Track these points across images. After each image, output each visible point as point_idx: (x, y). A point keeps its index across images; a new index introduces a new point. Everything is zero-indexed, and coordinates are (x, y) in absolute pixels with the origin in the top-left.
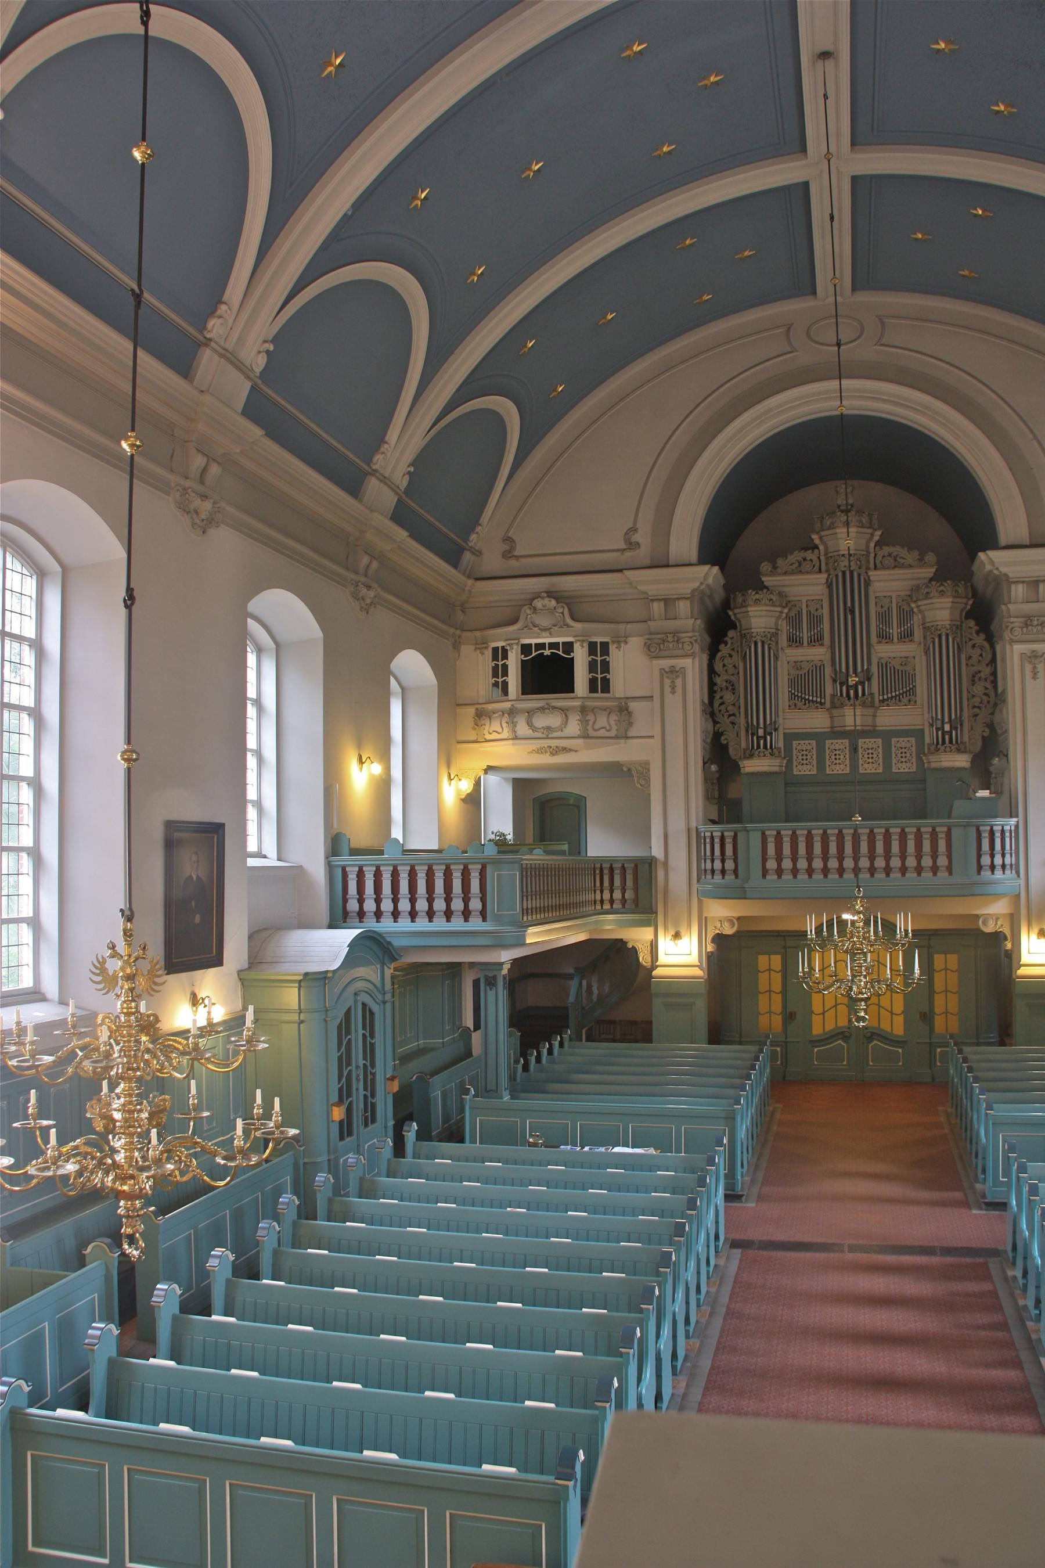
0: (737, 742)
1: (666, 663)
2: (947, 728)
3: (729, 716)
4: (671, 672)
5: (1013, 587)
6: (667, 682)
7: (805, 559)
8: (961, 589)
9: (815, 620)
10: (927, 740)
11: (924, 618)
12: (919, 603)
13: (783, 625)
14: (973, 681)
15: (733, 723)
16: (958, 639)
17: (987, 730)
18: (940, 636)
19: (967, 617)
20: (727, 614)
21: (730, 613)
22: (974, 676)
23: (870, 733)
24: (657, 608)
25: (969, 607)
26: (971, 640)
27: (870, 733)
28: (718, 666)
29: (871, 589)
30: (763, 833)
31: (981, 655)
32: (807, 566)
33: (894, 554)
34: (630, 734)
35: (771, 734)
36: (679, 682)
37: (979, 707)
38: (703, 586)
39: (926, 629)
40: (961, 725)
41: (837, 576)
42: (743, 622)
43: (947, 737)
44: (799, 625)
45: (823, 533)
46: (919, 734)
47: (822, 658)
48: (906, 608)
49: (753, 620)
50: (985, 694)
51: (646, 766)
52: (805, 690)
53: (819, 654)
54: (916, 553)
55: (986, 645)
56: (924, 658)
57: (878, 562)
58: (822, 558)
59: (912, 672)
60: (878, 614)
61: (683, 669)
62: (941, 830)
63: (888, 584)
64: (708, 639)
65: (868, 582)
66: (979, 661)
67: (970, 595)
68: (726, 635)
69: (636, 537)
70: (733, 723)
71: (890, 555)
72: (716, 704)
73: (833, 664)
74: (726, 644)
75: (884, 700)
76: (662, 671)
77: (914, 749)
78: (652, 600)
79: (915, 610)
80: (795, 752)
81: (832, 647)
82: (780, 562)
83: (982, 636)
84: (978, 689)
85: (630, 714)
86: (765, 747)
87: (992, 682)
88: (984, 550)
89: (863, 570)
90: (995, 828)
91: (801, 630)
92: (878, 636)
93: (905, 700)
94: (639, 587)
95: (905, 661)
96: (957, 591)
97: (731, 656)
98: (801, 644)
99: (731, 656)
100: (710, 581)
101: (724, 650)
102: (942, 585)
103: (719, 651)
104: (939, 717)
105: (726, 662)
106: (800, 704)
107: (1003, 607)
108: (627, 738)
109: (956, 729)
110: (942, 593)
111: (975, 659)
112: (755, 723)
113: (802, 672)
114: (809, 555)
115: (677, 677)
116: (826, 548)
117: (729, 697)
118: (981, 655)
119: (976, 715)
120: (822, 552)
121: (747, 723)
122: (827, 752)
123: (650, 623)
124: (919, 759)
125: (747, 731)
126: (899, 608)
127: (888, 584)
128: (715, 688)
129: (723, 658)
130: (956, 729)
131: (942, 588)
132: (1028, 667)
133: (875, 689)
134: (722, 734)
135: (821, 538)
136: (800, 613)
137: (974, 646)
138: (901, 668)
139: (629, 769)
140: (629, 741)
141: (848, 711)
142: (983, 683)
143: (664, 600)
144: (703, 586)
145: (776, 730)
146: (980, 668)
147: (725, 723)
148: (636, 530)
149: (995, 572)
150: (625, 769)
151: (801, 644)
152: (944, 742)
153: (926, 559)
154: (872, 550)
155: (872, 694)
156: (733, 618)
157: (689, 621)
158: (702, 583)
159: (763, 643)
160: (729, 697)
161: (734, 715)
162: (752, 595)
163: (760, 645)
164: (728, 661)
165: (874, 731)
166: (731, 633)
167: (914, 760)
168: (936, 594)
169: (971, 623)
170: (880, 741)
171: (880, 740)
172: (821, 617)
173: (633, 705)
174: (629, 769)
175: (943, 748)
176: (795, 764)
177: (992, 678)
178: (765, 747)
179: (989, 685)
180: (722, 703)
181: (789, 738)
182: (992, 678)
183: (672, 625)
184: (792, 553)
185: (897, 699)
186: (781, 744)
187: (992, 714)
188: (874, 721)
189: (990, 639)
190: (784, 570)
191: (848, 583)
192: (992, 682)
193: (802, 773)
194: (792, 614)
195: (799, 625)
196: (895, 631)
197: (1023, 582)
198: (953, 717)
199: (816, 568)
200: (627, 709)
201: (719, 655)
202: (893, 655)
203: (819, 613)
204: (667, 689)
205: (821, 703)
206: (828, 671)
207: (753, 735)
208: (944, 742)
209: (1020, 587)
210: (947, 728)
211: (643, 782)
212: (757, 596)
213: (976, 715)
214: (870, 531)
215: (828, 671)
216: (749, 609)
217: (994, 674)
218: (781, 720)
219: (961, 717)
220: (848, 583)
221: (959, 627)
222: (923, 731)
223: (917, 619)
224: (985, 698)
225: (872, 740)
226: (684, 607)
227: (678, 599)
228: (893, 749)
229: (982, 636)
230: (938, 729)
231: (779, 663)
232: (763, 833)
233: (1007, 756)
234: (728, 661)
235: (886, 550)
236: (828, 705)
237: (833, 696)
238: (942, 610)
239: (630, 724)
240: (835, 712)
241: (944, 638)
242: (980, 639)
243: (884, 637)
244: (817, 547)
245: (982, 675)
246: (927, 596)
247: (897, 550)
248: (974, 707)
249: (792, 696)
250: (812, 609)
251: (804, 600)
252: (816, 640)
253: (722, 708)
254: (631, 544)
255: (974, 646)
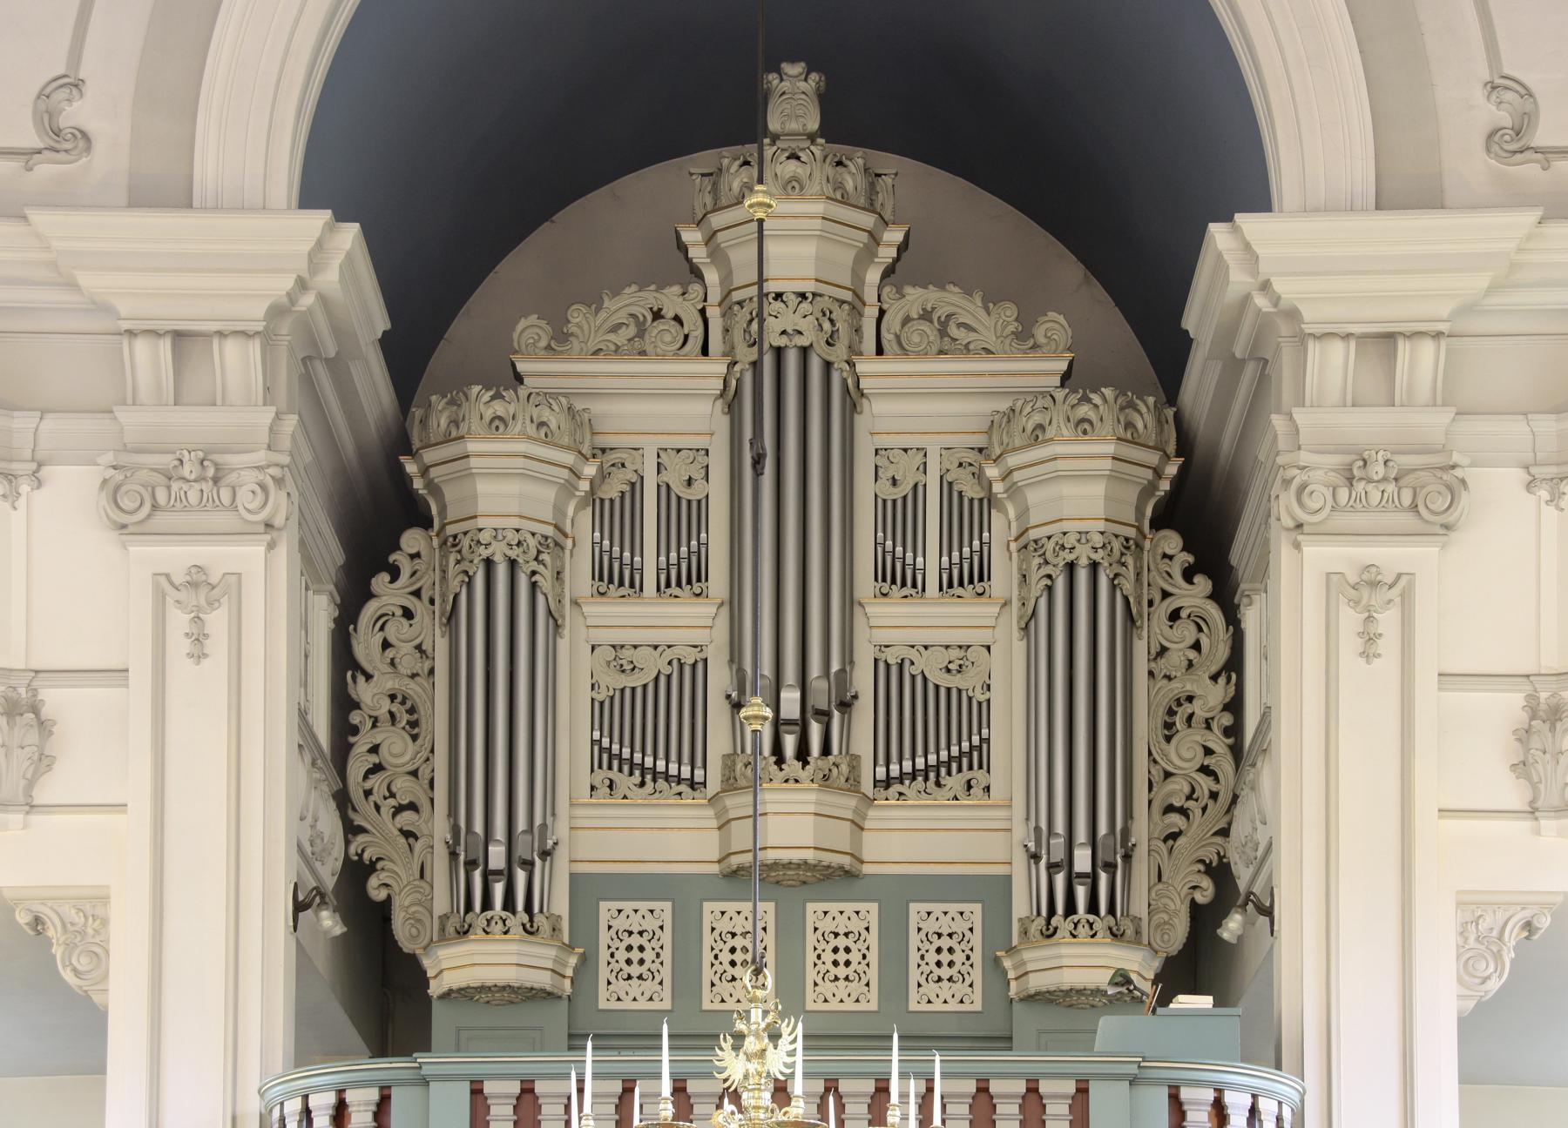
0: (418, 895)
1: (177, 556)
2: (1082, 861)
3: (399, 810)
4: (194, 585)
5: (1313, 348)
6: (179, 621)
7: (657, 315)
8: (1144, 420)
9: (685, 516)
10: (1021, 906)
11: (1023, 513)
12: (1013, 460)
13: (583, 527)
14: (1168, 726)
15: (408, 834)
16: (1128, 586)
17: (1207, 883)
18: (1071, 567)
19: (1157, 524)
20: (401, 467)
21: (411, 468)
22: (1171, 713)
23: (836, 878)
24: (149, 361)
25: (1165, 486)
26: (1166, 595)
27: (836, 878)
28: (365, 646)
29: (862, 423)
30: (477, 1092)
31: (1197, 646)
32: (665, 333)
33: (942, 312)
34: (42, 796)
35: (528, 865)
36: (217, 621)
37: (1183, 812)
38: (308, 300)
39: (1028, 546)
40: (1127, 857)
41: (756, 365)
42: (450, 493)
43: (1081, 893)
44: (635, 530)
45: (717, 220)
46: (994, 891)
47: (699, 637)
48: (972, 491)
49: (482, 487)
50: (1205, 770)
51: (95, 904)
52: (647, 735)
53: (690, 623)
54: (1009, 312)
55: (1214, 612)
56: (1019, 647)
57: (887, 337)
58: (713, 313)
59: (980, 696)
60: (880, 503)
61: (233, 584)
62: (1058, 1090)
63: (919, 407)
64: (333, 553)
65: (854, 399)
66: (1190, 664)
67: (1171, 448)
68: (396, 547)
69: (76, 113)
70: (408, 834)
71: (926, 316)
72: (358, 764)
73: (735, 656)
74: (395, 574)
75: (888, 782)
76: (163, 586)
77: (977, 940)
78: (131, 333)
79: (998, 488)
80: (604, 937)
81: (733, 603)
82: (578, 316)
83: (1203, 584)
84: (1184, 753)
85: (44, 727)
86: (509, 904)
87: (1227, 732)
88: (1228, 218)
89: (838, 354)
90: (1229, 1098)
91: (636, 546)
92: (881, 575)
93: (954, 782)
94: (85, 280)
95: (961, 657)
96: (1129, 425)
97: (408, 614)
98: (636, 586)
99: (408, 614)
100: (330, 278)
101: (387, 594)
102: (1085, 399)
103: (370, 596)
104: (1060, 827)
105: (391, 632)
106: (626, 782)
107: (1277, 421)
108: (32, 807)
109: (1110, 867)
110: (1083, 426)
111: (1178, 655)
112: (478, 827)
113: (636, 681)
114: (670, 300)
115: (212, 604)
116: (726, 277)
117: (397, 748)
118: (1197, 646)
119: (1174, 836)
120: (715, 295)
121: (455, 830)
122: (708, 940)
123: (125, 416)
124: (994, 965)
125: (453, 855)
126: (947, 487)
127: (919, 407)
128: (355, 718)
129: (382, 621)
130: (1110, 867)
131: (1084, 410)
132: (1349, 620)
133: (863, 743)
134: (371, 868)
135: (710, 239)
136: (635, 487)
137: (1175, 616)
138: (945, 681)
139: (37, 921)
140: (35, 819)
141: (775, 798)
142: (1198, 736)
143: (178, 336)
144: (308, 300)
145: (546, 854)
146: (1190, 687)
147: (381, 838)
148: (77, 85)
149: (1261, 302)
150: (22, 918)
151: (636, 586)
152: (1071, 908)
153: (1039, 334)
154: (870, 295)
155: (855, 761)
156: (418, 484)
157: (250, 419)
158: (302, 285)
159: (513, 563)
160: (397, 748)
161: (412, 807)
162: (482, 403)
163: (501, 572)
164: (397, 630)
165: (848, 875)
166: (412, 540)
167: (977, 975)
168: (1067, 432)
169: (1171, 541)
170: (871, 910)
171: (874, 907)
172: (702, 505)
173: (54, 698)
174: (37, 921)
175: (1068, 926)
176: (604, 973)
177: (1227, 720)
178: (509, 904)
179: (1219, 744)
180: (377, 768)
181: (587, 890)
182: (1227, 720)
183: (198, 424)
184: (616, 293)
185: (932, 775)
186: (561, 905)
187: (1224, 832)
188: (857, 842)
189: (1226, 597)
190: (592, 346)
191: (788, 402)
192: (1227, 732)
193: (627, 1004)
194: (612, 490)
195: (635, 530)
196: (932, 563)
197: (1347, 337)
198: (1103, 829)
199: (695, 344)
200: (35, 709)
201: (370, 610)
202: (921, 637)
203: (695, 493)
204: (178, 644)
205: (692, 785)
206: (719, 680)
207: (471, 864)
208: (1071, 908)
209: (1337, 350)
210: (1082, 861)
211: (83, 963)
212: (499, 408)
213: (1174, 836)
214: (868, 220)
215: (719, 680)
216: (472, 446)
217: (1235, 706)
218: (561, 830)
219: (1126, 832)
220: (788, 402)
221: (1133, 546)
222: (1007, 880)
223: (1001, 528)
224: (1206, 784)
225: (849, 907)
226: (238, 364)
227: (221, 334)
228: (914, 939)
229: (1203, 584)
230: (1052, 867)
231: (563, 644)
232: (477, 1092)
233: (1268, 912)
234: (397, 630)
235: (916, 297)
236: (714, 784)
237: (729, 761)
238: (1082, 484)
239: (43, 762)
240: (738, 804)
241: (1082, 576)
242: (1195, 596)
243: (897, 576)
244: (696, 273)
245: (1197, 707)
246: (1038, 435)
247: (949, 300)
248: (1169, 809)
249: (604, 757)
250: (676, 481)
251: (650, 447)
252: (686, 576)
253: (376, 782)
254: (57, 133)
255: (1175, 616)
